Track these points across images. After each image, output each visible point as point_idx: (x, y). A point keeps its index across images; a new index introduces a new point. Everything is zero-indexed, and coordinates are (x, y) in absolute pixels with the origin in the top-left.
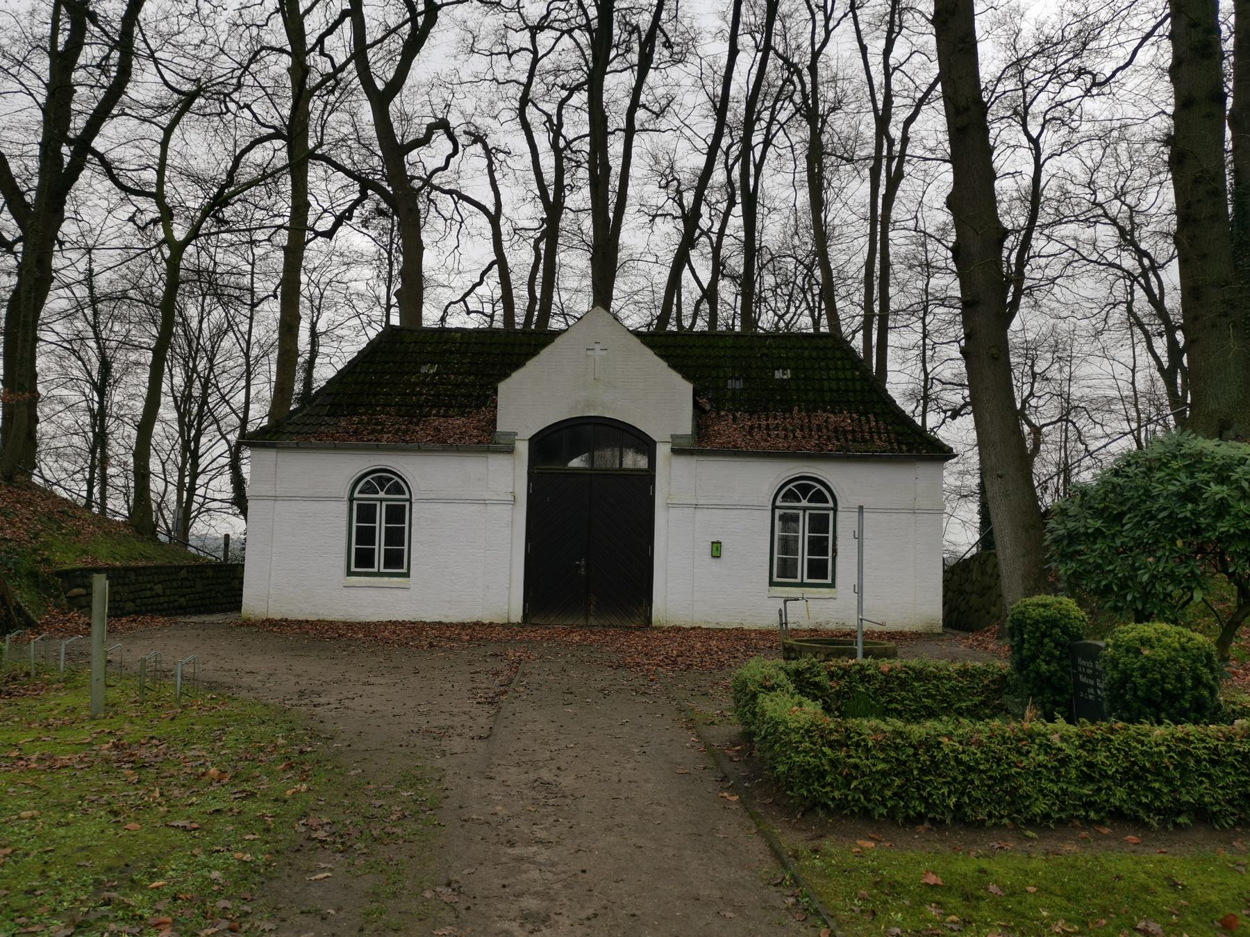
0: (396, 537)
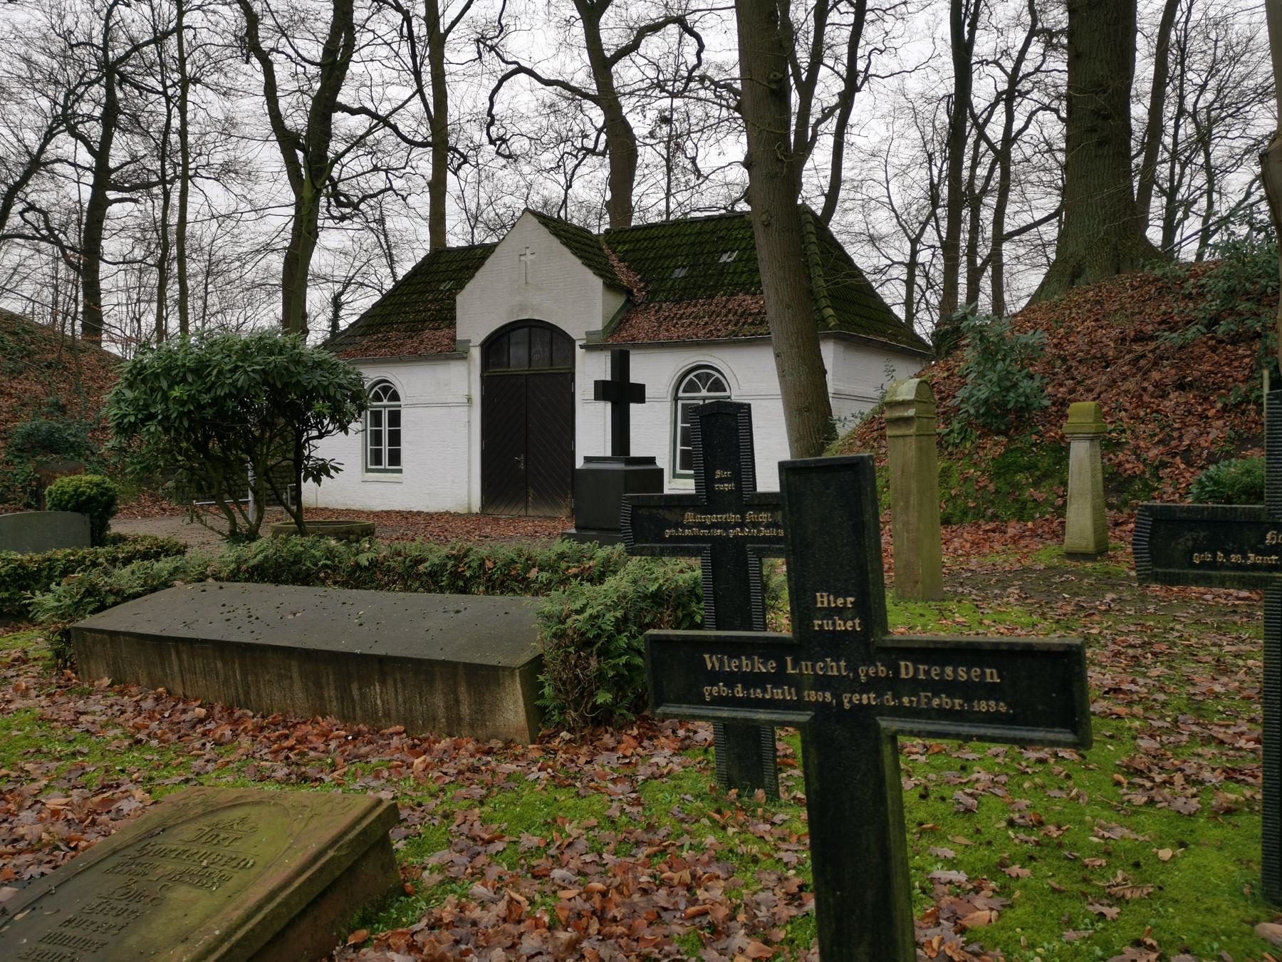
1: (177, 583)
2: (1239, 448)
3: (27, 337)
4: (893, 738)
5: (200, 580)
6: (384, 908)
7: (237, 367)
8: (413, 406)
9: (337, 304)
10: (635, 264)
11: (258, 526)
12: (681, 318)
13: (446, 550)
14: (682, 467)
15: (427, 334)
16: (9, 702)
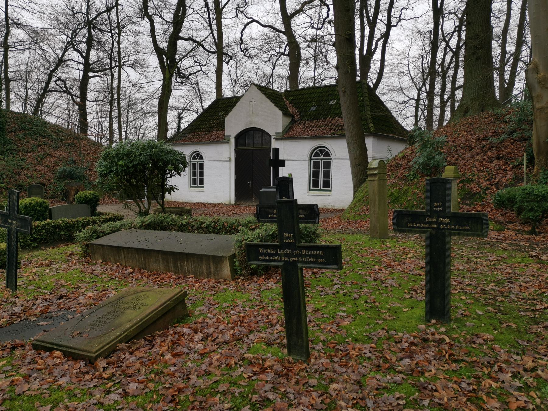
0: (327, 174)
1: (122, 229)
2: (517, 183)
3: (60, 134)
4: (301, 269)
5: (130, 229)
6: (183, 319)
7: (141, 154)
8: (208, 161)
9: (180, 118)
10: (296, 105)
11: (149, 210)
12: (313, 127)
13: (211, 220)
14: (313, 187)
15: (214, 133)
16: (70, 267)
